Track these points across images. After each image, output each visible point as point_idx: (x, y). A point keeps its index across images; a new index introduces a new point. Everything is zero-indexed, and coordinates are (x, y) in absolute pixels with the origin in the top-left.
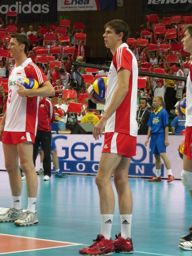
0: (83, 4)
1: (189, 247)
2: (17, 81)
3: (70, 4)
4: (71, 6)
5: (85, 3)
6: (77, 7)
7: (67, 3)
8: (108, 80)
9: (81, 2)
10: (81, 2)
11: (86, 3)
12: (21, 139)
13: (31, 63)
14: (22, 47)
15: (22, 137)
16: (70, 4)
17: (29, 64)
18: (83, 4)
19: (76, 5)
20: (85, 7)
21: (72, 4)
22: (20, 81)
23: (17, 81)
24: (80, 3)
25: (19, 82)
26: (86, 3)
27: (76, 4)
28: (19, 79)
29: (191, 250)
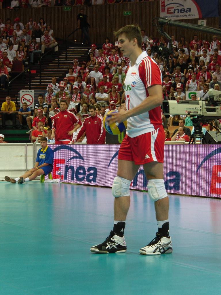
0: (185, 12)
1: (151, 252)
2: (132, 85)
3: (172, 13)
4: (173, 15)
5: (186, 12)
6: (180, 16)
7: (169, 12)
8: (164, 242)
9: (183, 11)
10: (183, 11)
11: (188, 11)
12: (86, 137)
13: (146, 57)
14: (134, 41)
15: (146, 156)
16: (172, 13)
17: (143, 60)
18: (185, 12)
19: (178, 14)
20: (187, 16)
21: (174, 12)
22: (135, 84)
23: (132, 85)
24: (182, 12)
25: (134, 85)
26: (188, 11)
27: (178, 12)
28: (133, 82)
29: (153, 255)
